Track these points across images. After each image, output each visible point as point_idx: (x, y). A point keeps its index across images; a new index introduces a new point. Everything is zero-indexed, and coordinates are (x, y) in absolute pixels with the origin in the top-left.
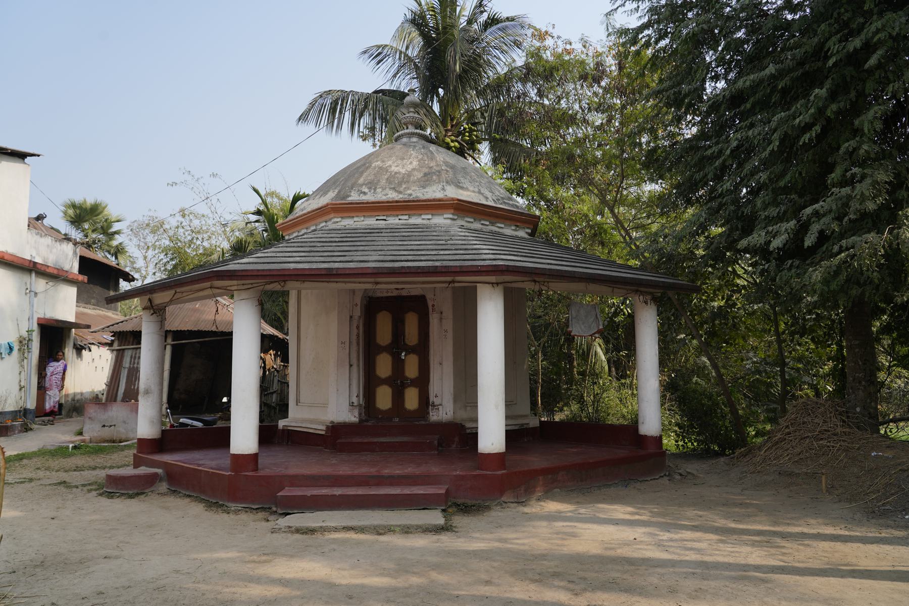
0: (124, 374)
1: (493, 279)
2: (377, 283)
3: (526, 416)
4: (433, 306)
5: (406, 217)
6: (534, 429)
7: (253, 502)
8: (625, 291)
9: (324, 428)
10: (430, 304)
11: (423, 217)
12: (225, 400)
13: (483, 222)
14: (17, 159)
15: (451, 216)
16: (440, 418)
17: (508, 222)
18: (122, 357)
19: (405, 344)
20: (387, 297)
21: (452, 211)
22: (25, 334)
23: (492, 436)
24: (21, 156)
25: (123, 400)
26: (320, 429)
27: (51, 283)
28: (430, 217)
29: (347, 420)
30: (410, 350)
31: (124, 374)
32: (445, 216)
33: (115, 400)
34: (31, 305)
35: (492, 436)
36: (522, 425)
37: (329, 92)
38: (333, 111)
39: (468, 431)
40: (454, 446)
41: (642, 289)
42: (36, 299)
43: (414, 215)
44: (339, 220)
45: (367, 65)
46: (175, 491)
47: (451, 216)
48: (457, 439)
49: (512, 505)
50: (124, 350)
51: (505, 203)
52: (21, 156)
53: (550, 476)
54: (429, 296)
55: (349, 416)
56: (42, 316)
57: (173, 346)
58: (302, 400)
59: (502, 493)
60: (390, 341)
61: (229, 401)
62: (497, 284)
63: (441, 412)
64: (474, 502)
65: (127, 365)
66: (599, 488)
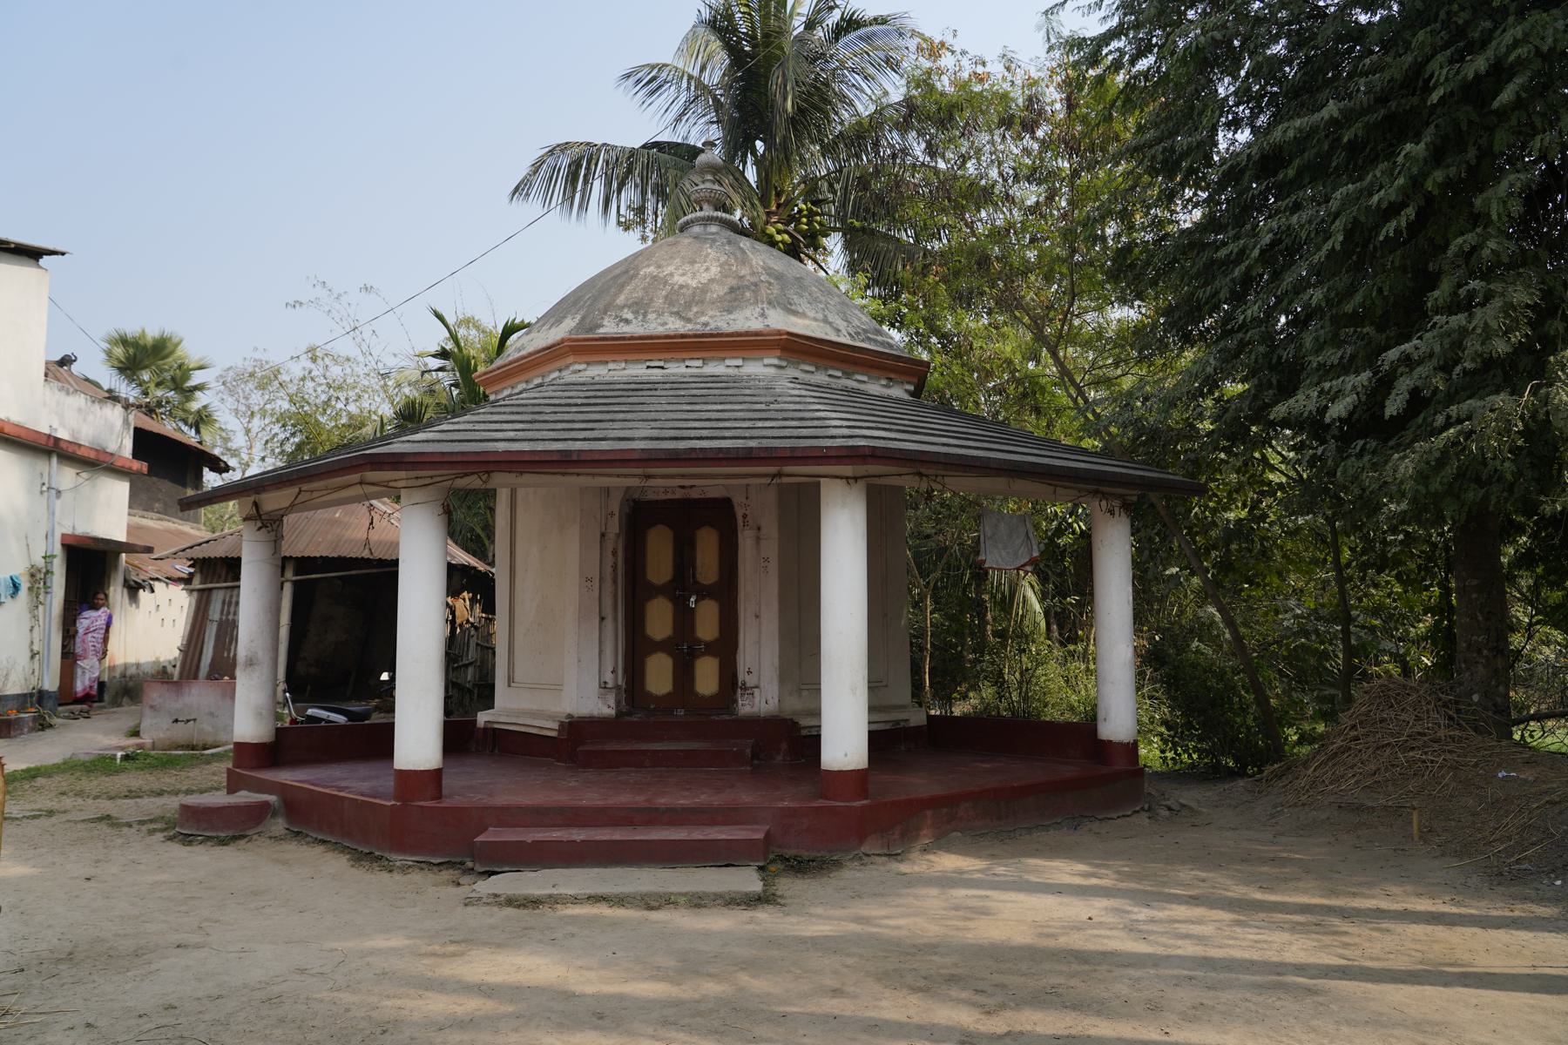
1: (847, 470)
2: (648, 477)
3: (903, 707)
4: (745, 516)
5: (699, 363)
6: (918, 728)
7: (433, 853)
9: (556, 726)
10: (739, 513)
11: (728, 362)
12: (385, 676)
14: (26, 259)
15: (776, 362)
16: (755, 709)
17: (875, 373)
18: (208, 602)
19: (696, 582)
20: (665, 501)
21: (778, 353)
22: (40, 563)
23: (844, 741)
24: (32, 254)
25: (210, 677)
26: (550, 727)
27: (84, 475)
28: (739, 362)
29: (596, 713)
30: (704, 593)
32: (766, 361)
33: (196, 677)
34: (51, 513)
35: (844, 741)
36: (898, 722)
37: (564, 147)
38: (572, 178)
39: (804, 732)
42: (58, 502)
44: (583, 366)
46: (298, 833)
47: (776, 362)
48: (784, 746)
49: (880, 860)
52: (32, 254)
54: (738, 499)
55: (602, 707)
57: (295, 583)
59: (862, 839)
60: (669, 578)
61: (393, 679)
63: (757, 700)
64: (813, 854)
66: (1029, 830)
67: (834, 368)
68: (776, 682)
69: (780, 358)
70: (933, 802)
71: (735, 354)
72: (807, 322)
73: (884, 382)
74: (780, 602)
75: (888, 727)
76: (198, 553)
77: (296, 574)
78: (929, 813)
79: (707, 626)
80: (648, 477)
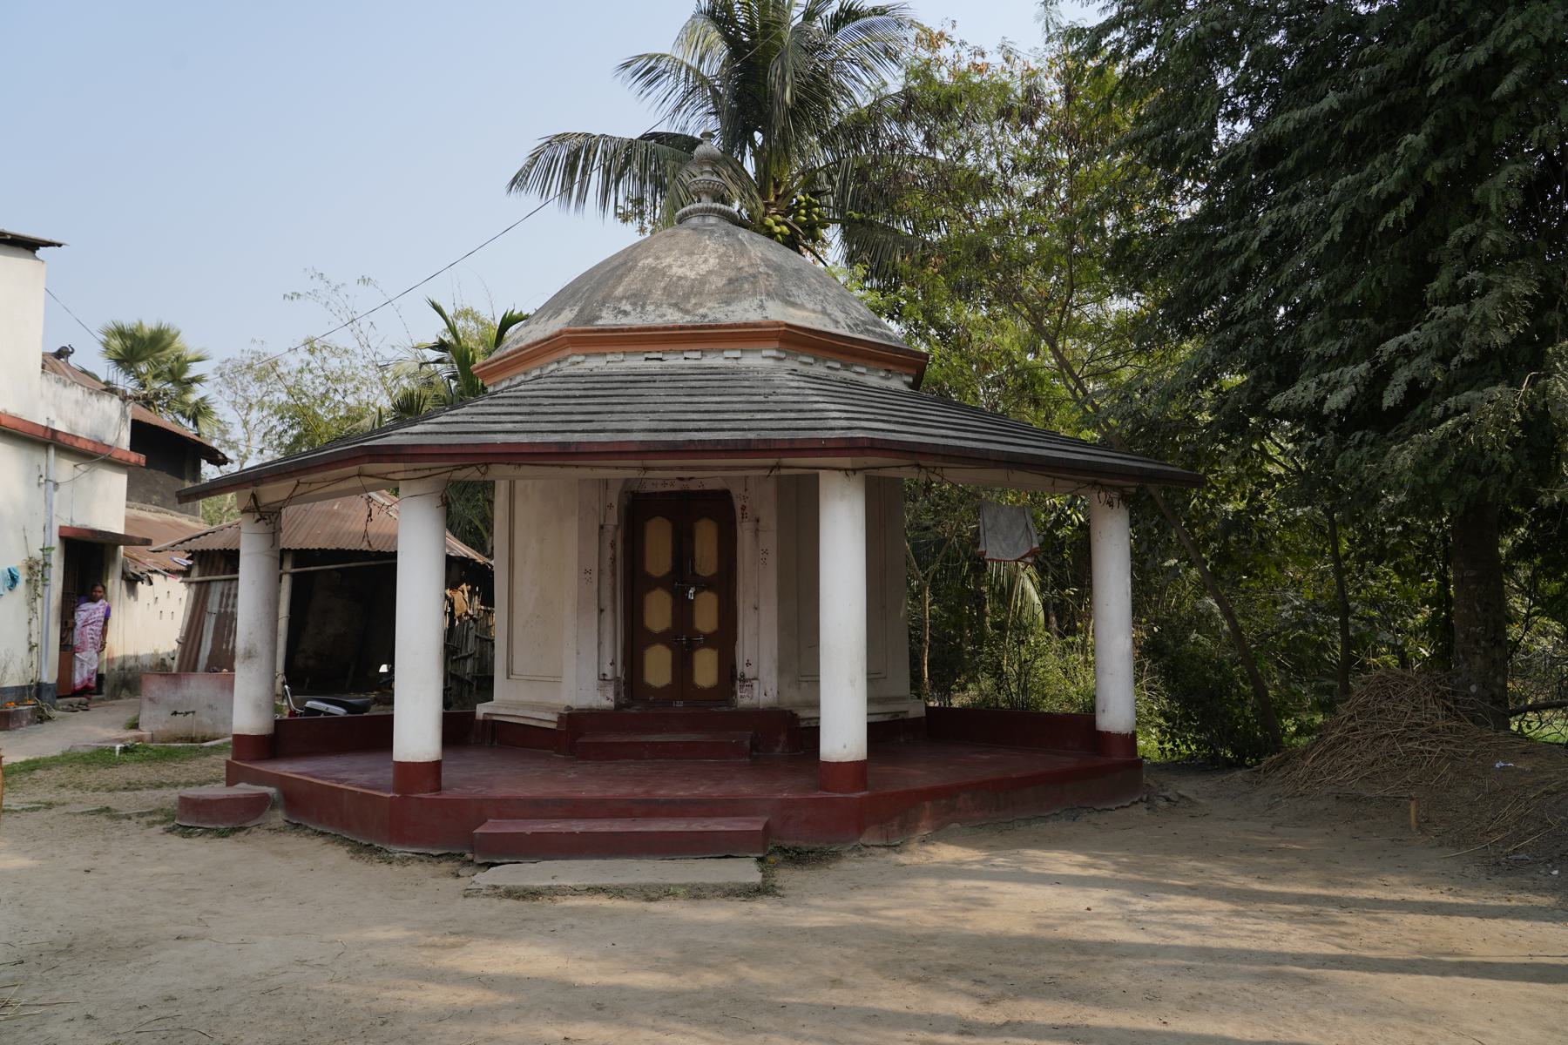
1: (846, 462)
2: (646, 469)
3: (903, 698)
4: (744, 508)
5: (698, 355)
9: (555, 718)
10: (738, 504)
11: (726, 354)
12: (384, 669)
13: (830, 364)
14: (22, 251)
15: (774, 353)
16: (754, 701)
17: (873, 365)
18: (207, 593)
19: (695, 574)
21: (777, 345)
22: (38, 555)
23: (843, 732)
24: (29, 245)
25: (208, 669)
27: (82, 467)
28: (737, 354)
32: (765, 353)
33: (194, 669)
35: (843, 732)
36: (896, 714)
37: (562, 138)
38: (571, 169)
39: (803, 724)
40: (778, 749)
42: (56, 494)
43: (711, 350)
47: (774, 353)
48: (783, 738)
50: (209, 582)
52: (29, 245)
54: (736, 492)
55: (602, 699)
58: (516, 670)
59: (860, 830)
60: (668, 569)
61: (391, 671)
63: (756, 692)
64: (813, 846)
65: (215, 609)
66: (1028, 821)
67: (803, 354)
68: (774, 674)
70: (932, 794)
72: (806, 314)
77: (294, 566)
80: (646, 469)
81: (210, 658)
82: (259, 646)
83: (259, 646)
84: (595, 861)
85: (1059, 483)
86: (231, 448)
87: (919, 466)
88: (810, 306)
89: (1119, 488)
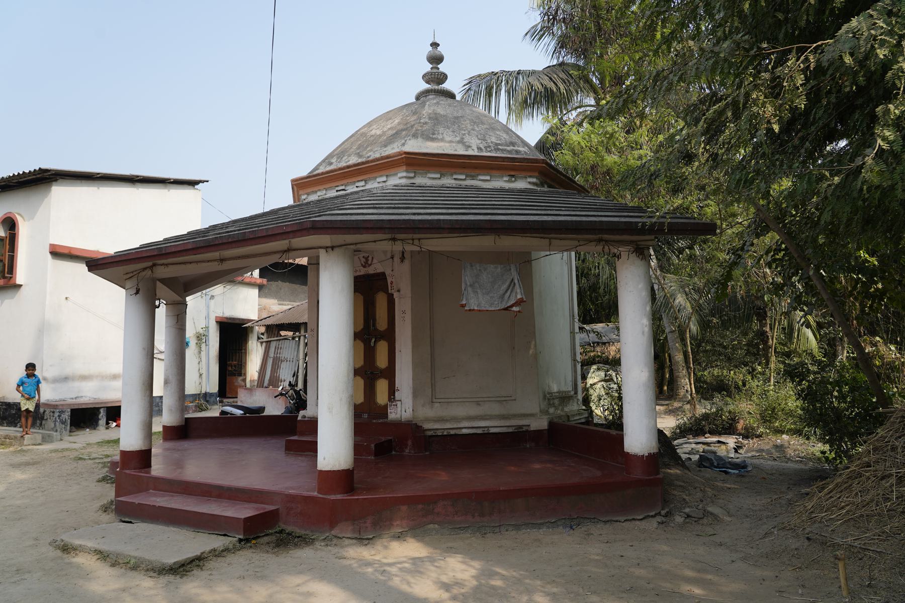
0: (270, 362)
2: (222, 260)
3: (532, 415)
5: (362, 183)
6: (539, 432)
8: (576, 243)
11: (379, 180)
13: (455, 177)
14: (128, 184)
15: (404, 174)
16: (398, 416)
17: (495, 173)
19: (376, 329)
21: (404, 168)
22: (201, 331)
24: (192, 183)
27: (228, 287)
28: (384, 179)
31: (270, 362)
32: (400, 175)
34: (208, 307)
36: (521, 427)
38: (489, 94)
39: (430, 433)
40: (407, 451)
41: (606, 236)
42: (212, 301)
43: (370, 179)
45: (528, 46)
47: (404, 174)
48: (410, 443)
49: (347, 542)
51: (499, 149)
52: (192, 183)
53: (420, 506)
56: (221, 315)
59: (332, 525)
60: (362, 327)
62: (333, 248)
63: (399, 409)
64: (303, 532)
66: (517, 527)
67: (456, 173)
68: (411, 396)
69: (407, 171)
71: (381, 173)
72: (442, 144)
73: (506, 179)
74: (413, 341)
75: (510, 430)
76: (269, 322)
78: (404, 508)
79: (382, 362)
80: (222, 260)
81: (270, 380)
82: (170, 377)
83: (170, 377)
84: (160, 527)
85: (554, 242)
86: (809, 278)
87: (394, 239)
88: (448, 139)
89: (631, 242)
